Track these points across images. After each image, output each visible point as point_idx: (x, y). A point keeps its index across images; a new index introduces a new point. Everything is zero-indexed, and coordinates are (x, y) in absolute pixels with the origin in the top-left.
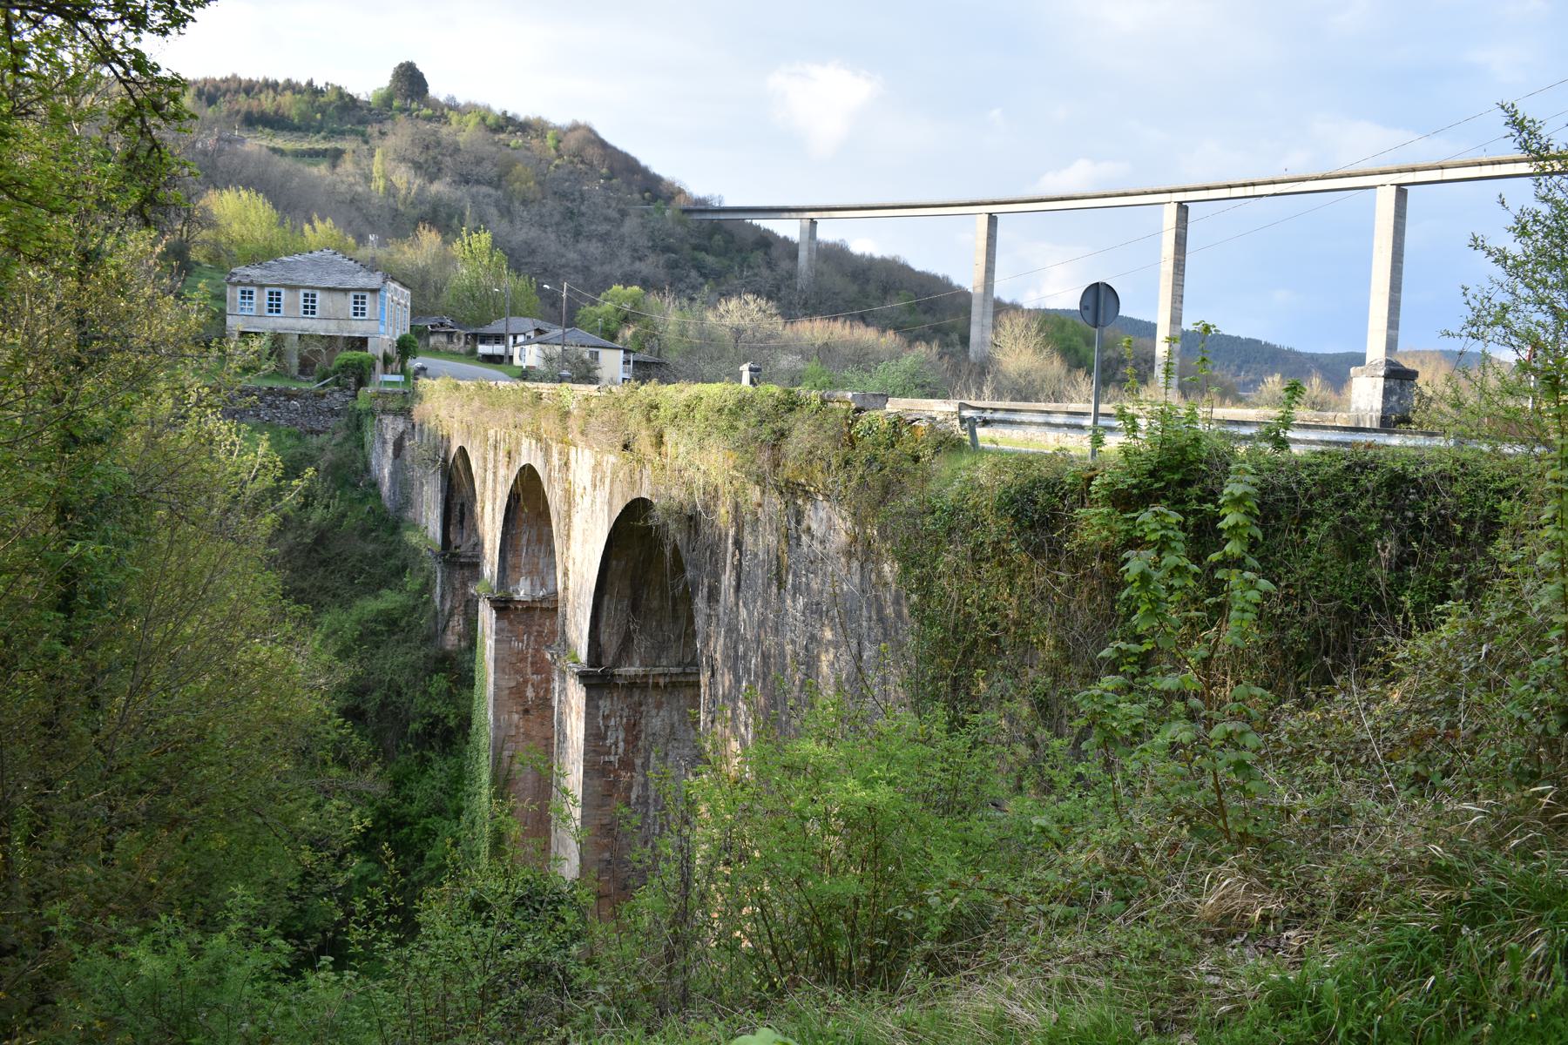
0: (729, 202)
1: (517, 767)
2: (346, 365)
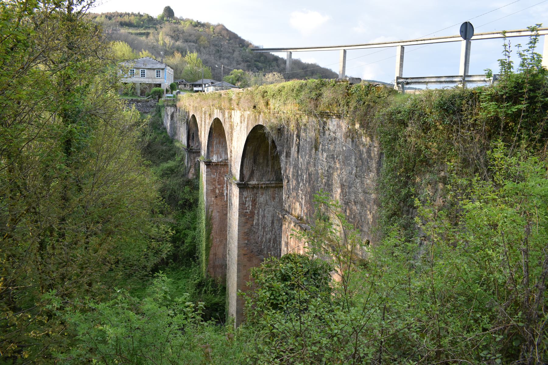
0: (265, 47)
1: (213, 214)
2: (155, 92)
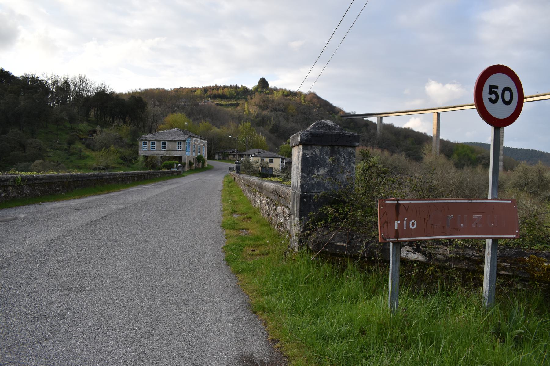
0: (357, 113)
